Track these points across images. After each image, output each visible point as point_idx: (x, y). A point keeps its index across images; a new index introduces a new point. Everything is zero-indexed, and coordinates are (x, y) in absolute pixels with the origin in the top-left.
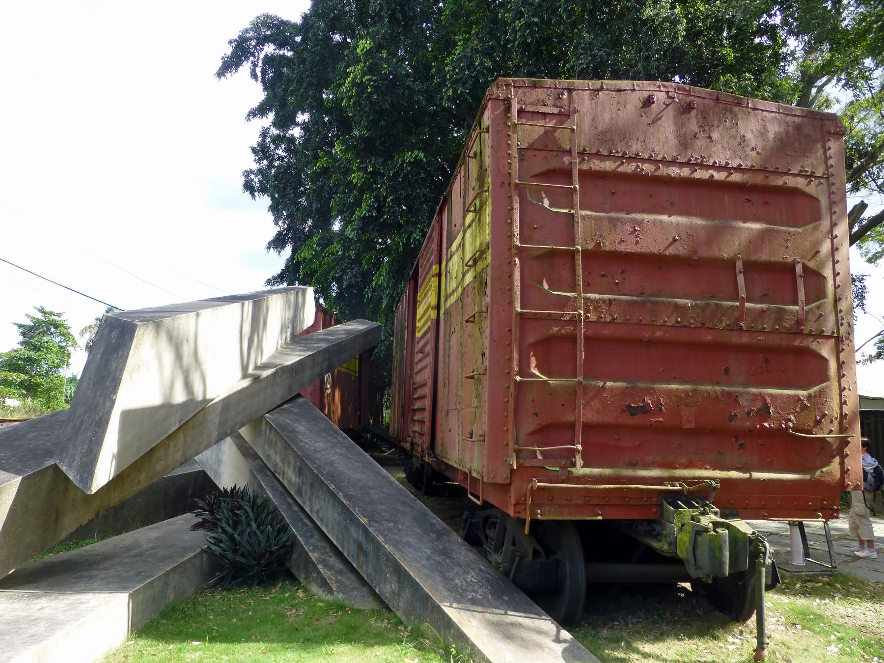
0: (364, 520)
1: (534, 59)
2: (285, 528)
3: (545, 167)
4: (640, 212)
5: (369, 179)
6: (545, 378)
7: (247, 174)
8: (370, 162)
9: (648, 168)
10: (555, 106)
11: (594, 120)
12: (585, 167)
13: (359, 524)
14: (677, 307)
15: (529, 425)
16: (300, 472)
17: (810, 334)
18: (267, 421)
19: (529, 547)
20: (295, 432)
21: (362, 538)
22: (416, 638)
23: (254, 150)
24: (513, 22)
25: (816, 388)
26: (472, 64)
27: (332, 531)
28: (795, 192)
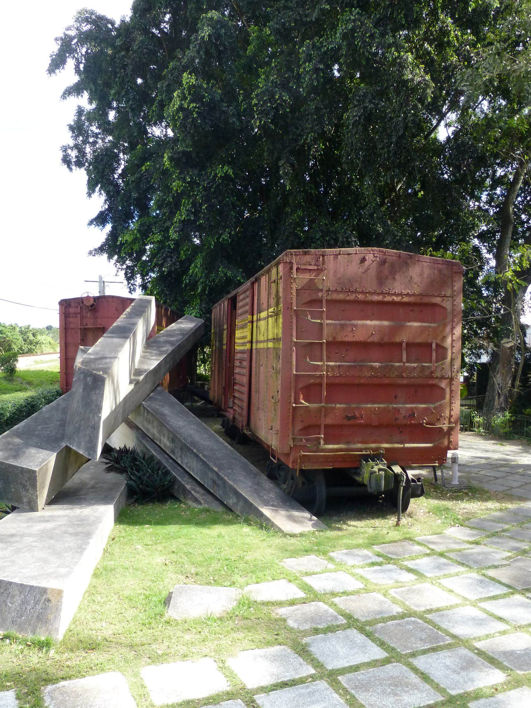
0: (216, 469)
1: (321, 96)
2: (167, 473)
3: (309, 299)
4: (355, 320)
5: (187, 187)
6: (308, 404)
7: (65, 149)
8: (188, 173)
9: (361, 297)
10: (315, 265)
11: (335, 272)
12: (329, 298)
13: (214, 471)
14: (372, 367)
15: (299, 426)
16: (173, 441)
17: (437, 378)
18: (144, 407)
19: (300, 480)
20: (164, 415)
21: (215, 478)
22: (248, 522)
23: (71, 128)
24: (304, 62)
25: (439, 403)
26: (273, 97)
27: (197, 474)
28: (435, 305)
